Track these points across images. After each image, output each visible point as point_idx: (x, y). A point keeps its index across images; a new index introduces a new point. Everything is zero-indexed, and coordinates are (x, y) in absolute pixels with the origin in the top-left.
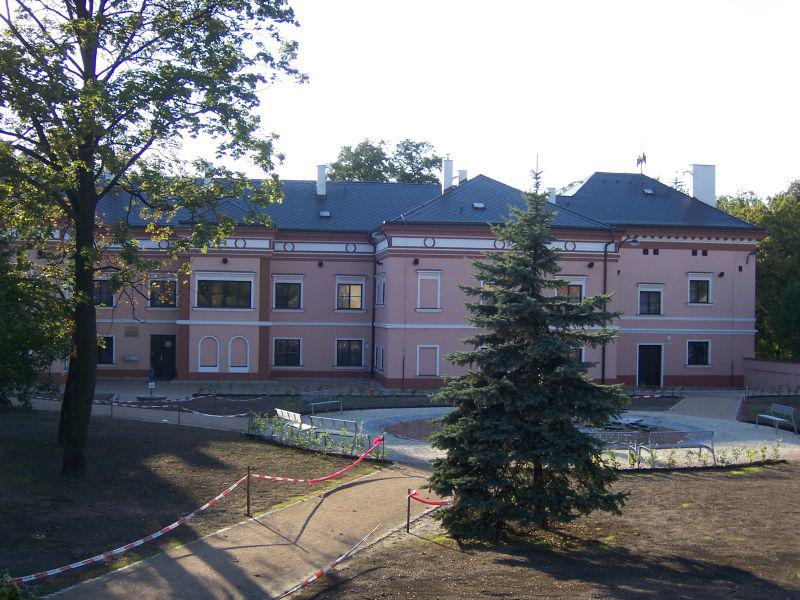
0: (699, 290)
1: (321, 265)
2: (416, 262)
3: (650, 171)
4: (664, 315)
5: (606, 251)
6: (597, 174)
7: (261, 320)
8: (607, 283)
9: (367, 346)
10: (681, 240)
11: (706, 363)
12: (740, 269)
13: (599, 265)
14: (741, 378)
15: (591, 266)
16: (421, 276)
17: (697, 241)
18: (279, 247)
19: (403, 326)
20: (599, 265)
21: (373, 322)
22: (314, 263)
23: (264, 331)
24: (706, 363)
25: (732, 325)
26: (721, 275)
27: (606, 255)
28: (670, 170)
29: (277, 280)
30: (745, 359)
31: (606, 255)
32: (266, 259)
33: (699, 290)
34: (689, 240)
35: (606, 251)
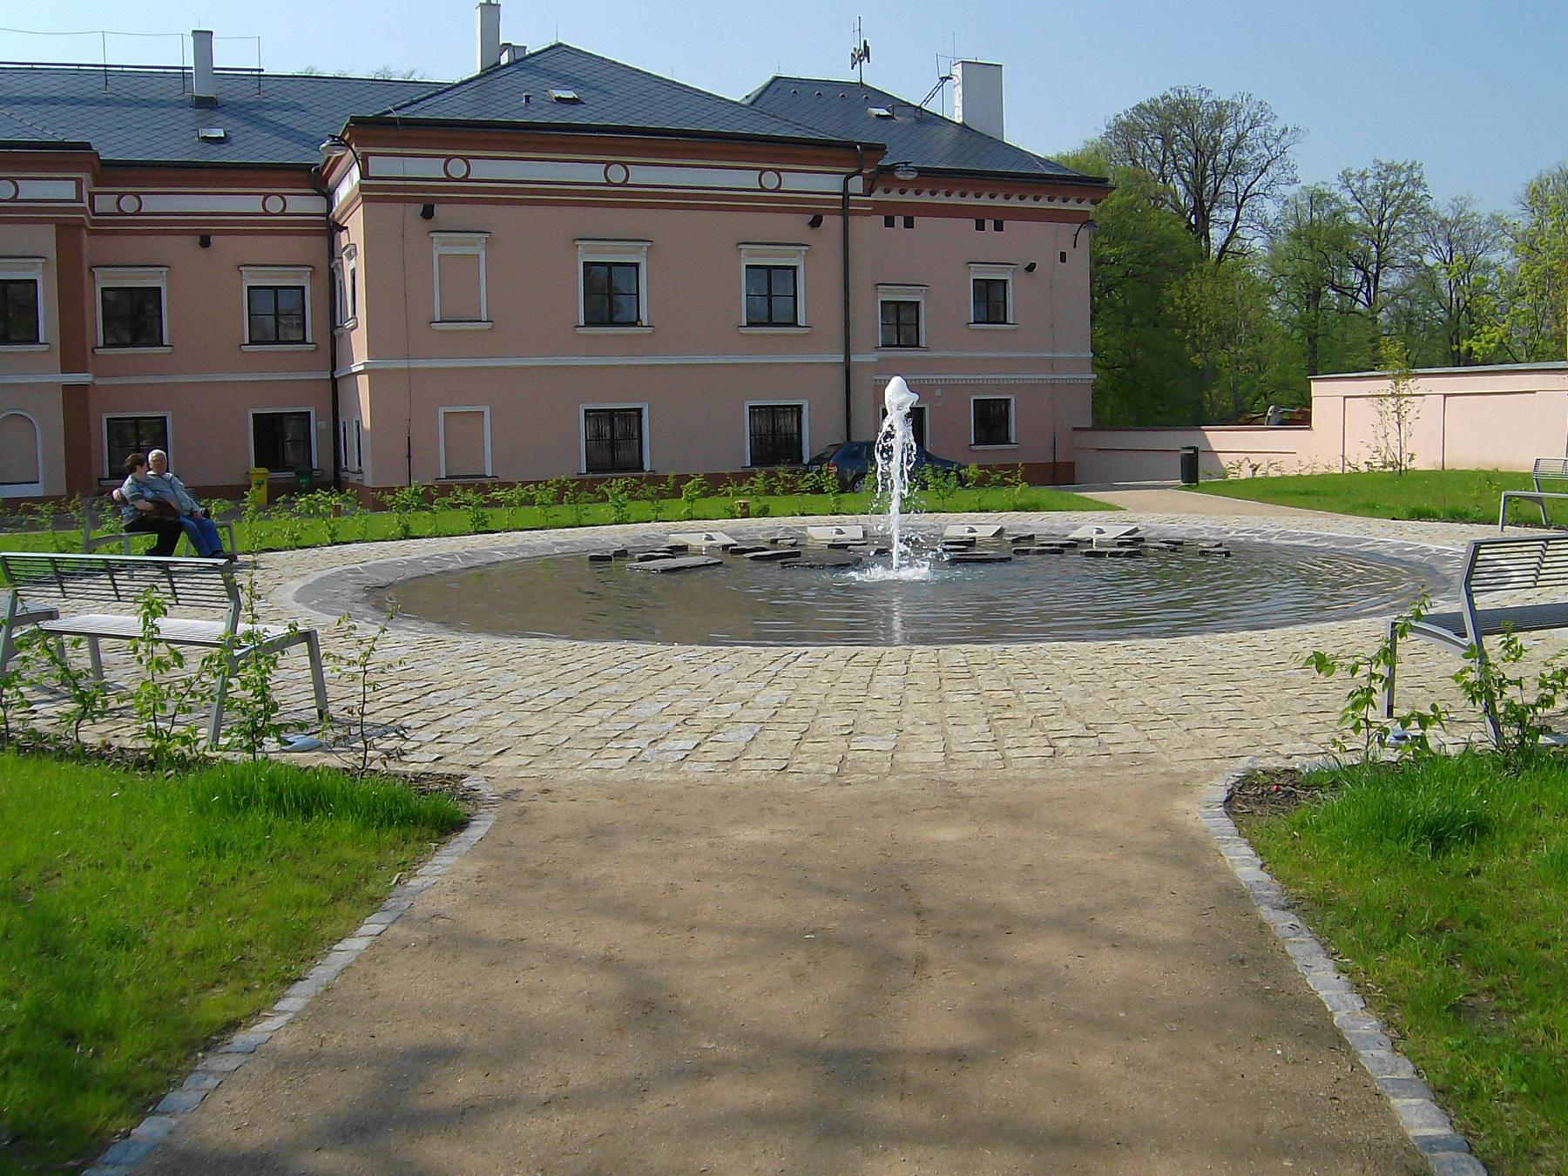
0: (990, 301)
1: (205, 242)
2: (428, 213)
3: (875, 76)
4: (927, 349)
5: (845, 193)
6: (777, 83)
7: (65, 370)
8: (840, 285)
9: (323, 425)
10: (955, 199)
11: (1007, 441)
12: (1063, 257)
13: (832, 223)
14: (1071, 465)
15: (816, 223)
16: (441, 246)
17: (984, 201)
18: (105, 204)
19: (403, 364)
20: (832, 223)
21: (334, 368)
22: (189, 239)
23: (75, 398)
24: (1007, 441)
25: (1052, 365)
26: (1031, 268)
27: (845, 202)
28: (915, 74)
29: (106, 279)
30: (1075, 429)
31: (845, 202)
32: (70, 229)
33: (990, 301)
34: (969, 200)
35: (845, 193)
